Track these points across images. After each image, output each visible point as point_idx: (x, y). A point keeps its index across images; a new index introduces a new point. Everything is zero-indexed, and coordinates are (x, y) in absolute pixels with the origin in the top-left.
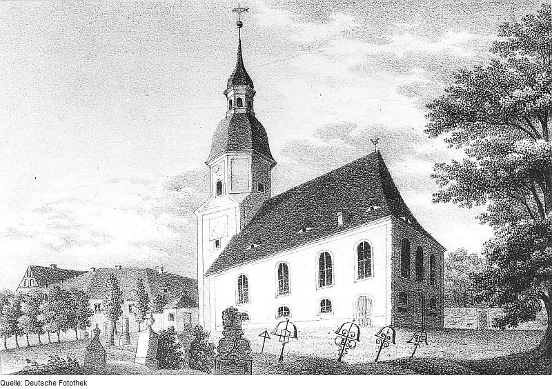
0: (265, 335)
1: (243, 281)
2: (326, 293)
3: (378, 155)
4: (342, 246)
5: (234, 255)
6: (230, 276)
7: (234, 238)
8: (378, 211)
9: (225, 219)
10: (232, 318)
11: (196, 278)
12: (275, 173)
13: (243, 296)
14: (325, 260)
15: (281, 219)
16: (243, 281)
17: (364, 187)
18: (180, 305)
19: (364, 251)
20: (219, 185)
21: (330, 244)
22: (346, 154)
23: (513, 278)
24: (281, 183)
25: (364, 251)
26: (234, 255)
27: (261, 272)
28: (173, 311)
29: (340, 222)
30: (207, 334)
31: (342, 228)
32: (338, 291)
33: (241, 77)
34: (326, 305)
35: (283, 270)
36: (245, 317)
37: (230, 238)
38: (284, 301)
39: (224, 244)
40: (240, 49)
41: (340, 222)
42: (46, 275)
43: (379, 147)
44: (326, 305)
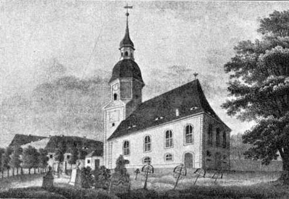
0: (137, 171)
1: (126, 144)
2: (170, 151)
3: (197, 81)
4: (177, 128)
5: (123, 129)
6: (120, 141)
7: (122, 122)
8: (197, 109)
9: (118, 113)
10: (121, 162)
11: (102, 141)
12: (144, 90)
13: (127, 152)
14: (169, 134)
15: (142, 116)
16: (126, 144)
17: (191, 97)
18: (94, 155)
19: (189, 129)
20: (115, 96)
21: (151, 132)
22: (185, 80)
23: (261, 144)
24: (145, 98)
25: (189, 129)
26: (123, 129)
27: (136, 139)
28: (90, 159)
29: (177, 114)
30: (230, 130)
31: (178, 117)
32: (169, 150)
33: (127, 43)
34: (169, 157)
35: (147, 139)
36: (127, 162)
37: (121, 121)
38: (148, 154)
39: (117, 124)
40: (127, 27)
41: (177, 114)
42: (248, 41)
43: (198, 77)
44: (169, 157)
